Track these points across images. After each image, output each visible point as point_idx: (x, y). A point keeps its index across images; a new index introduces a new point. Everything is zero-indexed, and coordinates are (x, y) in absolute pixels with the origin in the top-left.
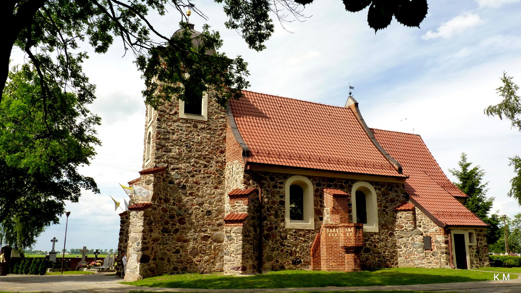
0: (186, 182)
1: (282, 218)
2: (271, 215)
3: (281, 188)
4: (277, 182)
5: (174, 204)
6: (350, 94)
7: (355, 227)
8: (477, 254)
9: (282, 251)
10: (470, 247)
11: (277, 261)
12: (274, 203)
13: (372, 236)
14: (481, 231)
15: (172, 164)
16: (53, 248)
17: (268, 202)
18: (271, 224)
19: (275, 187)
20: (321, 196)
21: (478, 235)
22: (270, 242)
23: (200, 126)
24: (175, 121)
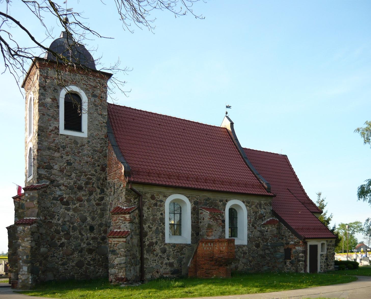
6: (227, 113)
8: (326, 261)
10: (321, 255)
16: (45, 48)
20: (60, 17)
21: (328, 245)
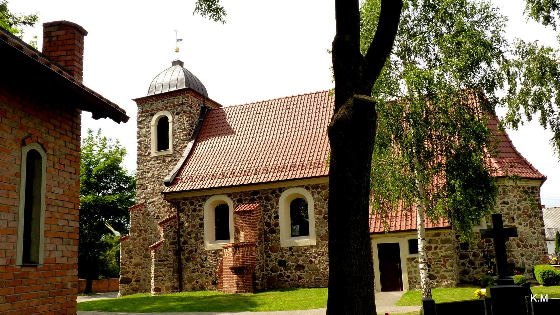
0: (159, 213)
1: (202, 241)
2: (191, 238)
3: (200, 210)
4: (196, 206)
5: (151, 234)
7: (233, 246)
9: (202, 272)
11: (197, 282)
12: (194, 226)
13: (308, 250)
14: (438, 235)
15: (148, 199)
17: (188, 227)
18: (191, 247)
19: (195, 210)
22: (191, 264)
23: (169, 159)
24: (149, 161)
